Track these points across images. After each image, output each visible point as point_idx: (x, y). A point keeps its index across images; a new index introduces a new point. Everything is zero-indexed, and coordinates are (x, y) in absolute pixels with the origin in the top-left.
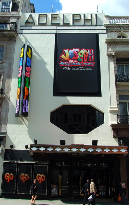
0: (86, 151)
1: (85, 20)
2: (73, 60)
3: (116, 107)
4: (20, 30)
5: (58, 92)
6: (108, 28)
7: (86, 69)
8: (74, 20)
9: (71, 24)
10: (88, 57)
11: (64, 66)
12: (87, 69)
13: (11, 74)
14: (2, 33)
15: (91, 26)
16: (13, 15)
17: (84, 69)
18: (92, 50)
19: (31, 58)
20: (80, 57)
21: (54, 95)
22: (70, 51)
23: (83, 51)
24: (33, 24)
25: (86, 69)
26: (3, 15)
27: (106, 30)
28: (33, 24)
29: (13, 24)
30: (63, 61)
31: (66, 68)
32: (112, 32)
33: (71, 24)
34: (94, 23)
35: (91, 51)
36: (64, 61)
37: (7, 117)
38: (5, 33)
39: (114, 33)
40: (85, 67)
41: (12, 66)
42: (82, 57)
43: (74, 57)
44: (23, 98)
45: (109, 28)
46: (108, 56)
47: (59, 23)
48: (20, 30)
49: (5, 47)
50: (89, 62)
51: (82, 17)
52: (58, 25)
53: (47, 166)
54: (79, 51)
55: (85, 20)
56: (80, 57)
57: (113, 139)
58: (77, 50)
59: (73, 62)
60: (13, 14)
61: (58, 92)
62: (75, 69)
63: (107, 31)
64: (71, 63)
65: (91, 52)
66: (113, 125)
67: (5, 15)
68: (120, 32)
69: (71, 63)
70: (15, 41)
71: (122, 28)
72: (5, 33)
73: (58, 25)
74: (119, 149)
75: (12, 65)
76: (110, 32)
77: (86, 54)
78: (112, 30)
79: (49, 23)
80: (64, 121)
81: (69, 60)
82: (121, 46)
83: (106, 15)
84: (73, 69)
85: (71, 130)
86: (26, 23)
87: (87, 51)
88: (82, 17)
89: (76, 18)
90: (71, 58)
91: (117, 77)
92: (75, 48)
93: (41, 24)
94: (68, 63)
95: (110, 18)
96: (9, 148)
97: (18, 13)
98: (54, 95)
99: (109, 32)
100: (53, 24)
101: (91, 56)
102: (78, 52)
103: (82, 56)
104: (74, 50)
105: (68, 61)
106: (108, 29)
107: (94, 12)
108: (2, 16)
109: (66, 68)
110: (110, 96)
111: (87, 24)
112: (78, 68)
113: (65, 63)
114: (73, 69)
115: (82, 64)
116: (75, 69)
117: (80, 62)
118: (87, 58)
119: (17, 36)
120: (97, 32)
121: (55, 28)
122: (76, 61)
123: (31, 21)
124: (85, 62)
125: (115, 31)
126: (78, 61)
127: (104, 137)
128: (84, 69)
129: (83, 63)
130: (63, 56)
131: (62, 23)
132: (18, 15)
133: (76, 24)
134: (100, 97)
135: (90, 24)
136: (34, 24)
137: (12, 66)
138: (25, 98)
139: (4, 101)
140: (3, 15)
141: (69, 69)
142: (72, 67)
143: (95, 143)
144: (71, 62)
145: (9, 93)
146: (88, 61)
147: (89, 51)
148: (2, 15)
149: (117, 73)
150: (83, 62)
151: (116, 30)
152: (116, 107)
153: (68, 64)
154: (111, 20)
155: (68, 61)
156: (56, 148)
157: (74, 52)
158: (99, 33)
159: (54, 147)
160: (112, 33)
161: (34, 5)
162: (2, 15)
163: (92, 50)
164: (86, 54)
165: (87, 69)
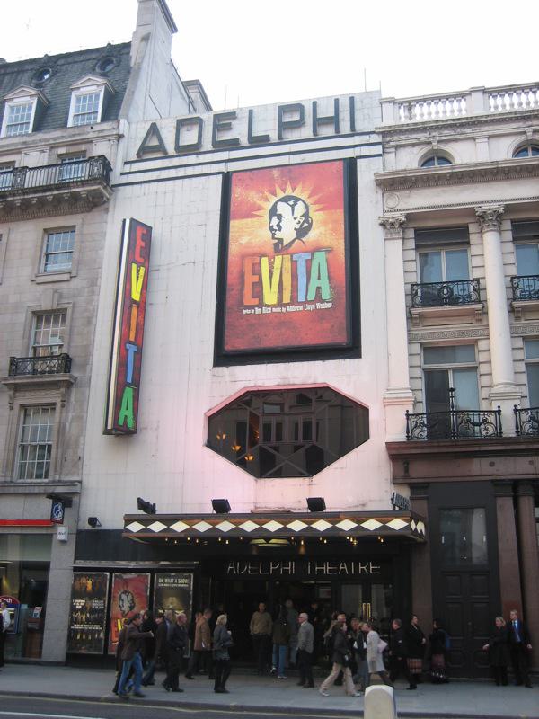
0: (146, 530)
1: (318, 122)
3: (407, 389)
4: (122, 174)
5: (224, 357)
6: (388, 139)
8: (283, 127)
9: (274, 137)
13: (94, 310)
14: (66, 191)
16: (100, 134)
21: (359, 355)
24: (161, 148)
26: (74, 135)
29: (97, 161)
33: (274, 137)
34: (345, 127)
37: (82, 438)
39: (408, 150)
41: (96, 285)
45: (389, 137)
46: (385, 226)
48: (122, 174)
49: (77, 229)
52: (234, 145)
53: (192, 575)
61: (224, 357)
63: (383, 148)
66: (389, 446)
67: (79, 134)
68: (430, 147)
70: (107, 210)
71: (434, 134)
72: (73, 190)
73: (234, 145)
74: (214, 524)
76: (397, 147)
78: (404, 143)
79: (207, 144)
82: (427, 191)
83: (384, 95)
85: (264, 467)
86: (138, 154)
89: (290, 117)
91: (515, 285)
93: (183, 151)
96: (88, 527)
97: (115, 125)
98: (359, 355)
99: (393, 150)
100: (219, 146)
106: (388, 142)
108: (69, 139)
110: (389, 355)
119: (110, 194)
123: (155, 142)
125: (414, 145)
127: (357, 487)
131: (244, 141)
133: (289, 136)
134: (348, 362)
135: (329, 131)
136: (165, 152)
137: (96, 285)
139: (73, 390)
140: (63, 137)
143: (316, 505)
145: (88, 367)
148: (70, 137)
149: (513, 271)
151: (414, 141)
152: (407, 389)
154: (492, 101)
156: (364, 521)
159: (190, 518)
160: (402, 152)
161: (200, 85)
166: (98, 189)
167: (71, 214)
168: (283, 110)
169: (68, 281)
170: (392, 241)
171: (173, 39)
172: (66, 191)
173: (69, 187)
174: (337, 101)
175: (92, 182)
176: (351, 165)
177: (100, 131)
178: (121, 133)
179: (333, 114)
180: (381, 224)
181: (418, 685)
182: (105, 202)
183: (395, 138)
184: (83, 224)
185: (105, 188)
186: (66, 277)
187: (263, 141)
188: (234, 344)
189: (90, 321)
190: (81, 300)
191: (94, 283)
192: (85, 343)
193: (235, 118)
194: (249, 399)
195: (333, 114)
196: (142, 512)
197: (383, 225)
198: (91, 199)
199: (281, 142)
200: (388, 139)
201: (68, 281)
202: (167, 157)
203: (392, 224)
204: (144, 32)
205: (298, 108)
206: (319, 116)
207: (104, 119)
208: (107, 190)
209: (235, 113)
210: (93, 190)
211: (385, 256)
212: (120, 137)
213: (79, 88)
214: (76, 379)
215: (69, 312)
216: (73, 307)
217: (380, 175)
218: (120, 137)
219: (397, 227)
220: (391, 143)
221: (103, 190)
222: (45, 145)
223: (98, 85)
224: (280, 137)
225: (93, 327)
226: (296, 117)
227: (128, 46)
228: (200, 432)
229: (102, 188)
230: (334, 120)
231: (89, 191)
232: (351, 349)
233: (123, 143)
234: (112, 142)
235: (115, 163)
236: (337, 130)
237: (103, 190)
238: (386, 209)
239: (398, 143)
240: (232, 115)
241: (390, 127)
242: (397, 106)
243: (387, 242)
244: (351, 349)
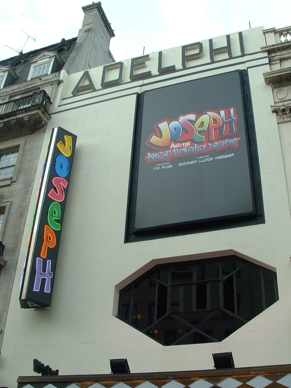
1: (214, 52)
2: (181, 142)
3: (3, 107)
5: (134, 233)
7: (216, 158)
8: (186, 59)
9: (179, 66)
10: (221, 128)
11: (155, 162)
12: (220, 157)
14: (13, 118)
15: (231, 58)
17: (211, 159)
18: (232, 110)
19: (71, 160)
20: (199, 132)
22: (174, 124)
23: (206, 118)
24: (91, 87)
25: (216, 158)
26: (27, 86)
27: (268, 58)
28: (91, 87)
30: (152, 152)
31: (161, 166)
32: (285, 61)
33: (179, 66)
34: (236, 50)
35: (230, 111)
36: (156, 149)
38: (18, 116)
40: (214, 153)
42: (205, 131)
43: (186, 133)
44: (37, 253)
47: (150, 72)
49: (20, 149)
50: (224, 139)
51: (206, 46)
54: (197, 119)
55: (214, 52)
56: (199, 132)
57: (114, 287)
58: (192, 117)
59: (180, 148)
60: (47, 80)
61: (134, 233)
62: (185, 164)
64: (174, 151)
65: (228, 115)
67: (31, 85)
69: (174, 151)
72: (18, 116)
73: (148, 75)
75: (32, 186)
77: (215, 121)
80: (156, 311)
81: (170, 144)
84: (180, 164)
87: (219, 114)
88: (206, 46)
89: (191, 52)
90: (174, 139)
92: (184, 114)
93: (106, 85)
94: (166, 153)
95: (278, 35)
99: (279, 61)
100: (134, 78)
101: (230, 123)
102: (193, 122)
103: (205, 127)
104: (182, 119)
105: (167, 148)
107: (233, 30)
109: (161, 166)
111: (218, 58)
112: (194, 160)
113: (159, 154)
114: (180, 164)
115: (205, 147)
116: (185, 164)
117: (199, 143)
118: (219, 131)
119: (48, 120)
120: (242, 67)
121: (140, 82)
122: (188, 144)
124: (212, 142)
126: (193, 142)
128: (211, 159)
129: (207, 146)
130: (154, 139)
131: (155, 72)
132: (56, 79)
135: (226, 56)
138: (44, 253)
141: (171, 166)
142: (175, 160)
144: (176, 149)
146: (221, 137)
147: (222, 113)
150: (209, 142)
152: (3, 107)
153: (167, 155)
155: (167, 148)
157: (183, 125)
158: (248, 68)
162: (24, 87)
163: (232, 110)
164: (215, 121)
165: (220, 157)
166: (37, 114)
167: (18, 137)
168: (185, 48)
169: (9, 185)
170: (284, 124)
171: (111, 40)
172: (13, 118)
173: (16, 115)
174: (228, 37)
175: (33, 108)
176: (243, 76)
177: (45, 80)
178: (61, 79)
179: (226, 45)
180: (273, 112)
181: (45, 366)
182: (43, 126)
183: (279, 53)
184: (25, 143)
185: (43, 113)
186: (8, 182)
187: (172, 69)
188: (141, 224)
189: (22, 215)
190: (16, 201)
191: (28, 186)
192: (16, 232)
193: (149, 59)
194: (158, 270)
195: (226, 45)
196: (36, 374)
197: (275, 111)
198: (32, 123)
199: (185, 68)
200: (273, 55)
201: (9, 185)
202: (95, 90)
203: (284, 111)
204: (87, 28)
205: (199, 45)
206: (214, 48)
207: (53, 72)
208: (45, 116)
209: (149, 55)
210: (34, 114)
211: (280, 136)
212: (59, 82)
213: (36, 62)
214: (6, 263)
215: (7, 209)
216: (10, 205)
217: (268, 74)
218: (59, 82)
219: (288, 112)
220: (276, 57)
221: (41, 114)
222: (6, 95)
223: (50, 58)
224: (183, 64)
225: (24, 219)
226: (197, 51)
227: (75, 40)
228: (109, 301)
229: (40, 113)
230: (228, 49)
231: (30, 116)
232: (254, 216)
233: (61, 86)
234: (54, 86)
235: (54, 99)
236: (230, 53)
237: (41, 114)
238: (277, 100)
239: (282, 57)
240: (147, 58)
241: (273, 45)
242: (278, 35)
243: (280, 125)
244: (254, 216)
